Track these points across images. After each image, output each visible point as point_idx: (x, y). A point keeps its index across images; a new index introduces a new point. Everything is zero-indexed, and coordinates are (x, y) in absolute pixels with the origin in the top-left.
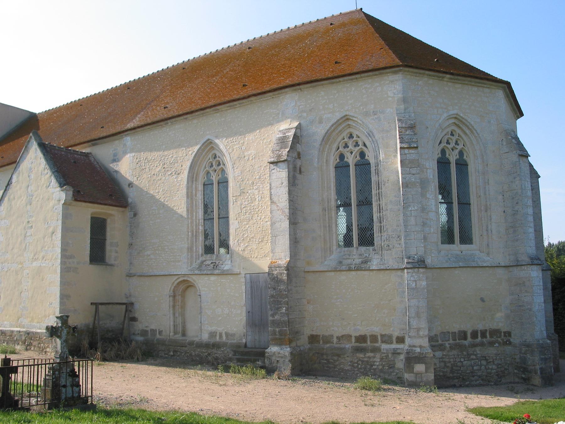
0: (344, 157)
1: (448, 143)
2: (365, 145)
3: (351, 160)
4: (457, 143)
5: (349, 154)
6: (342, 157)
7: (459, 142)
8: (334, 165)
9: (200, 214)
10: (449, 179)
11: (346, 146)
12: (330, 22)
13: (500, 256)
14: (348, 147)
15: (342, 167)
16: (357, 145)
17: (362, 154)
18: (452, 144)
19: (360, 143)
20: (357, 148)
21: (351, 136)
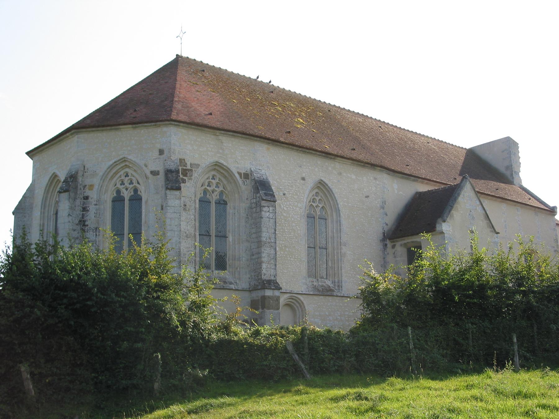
0: (137, 191)
1: (209, 185)
2: (138, 183)
3: (127, 195)
4: (217, 186)
5: (124, 190)
6: (118, 192)
7: (219, 185)
8: (111, 200)
9: (51, 227)
10: (209, 215)
11: (123, 183)
12: (304, 175)
13: (245, 285)
14: (133, 184)
15: (118, 200)
16: (131, 183)
17: (136, 190)
18: (213, 187)
19: (134, 181)
20: (131, 186)
21: (127, 175)
